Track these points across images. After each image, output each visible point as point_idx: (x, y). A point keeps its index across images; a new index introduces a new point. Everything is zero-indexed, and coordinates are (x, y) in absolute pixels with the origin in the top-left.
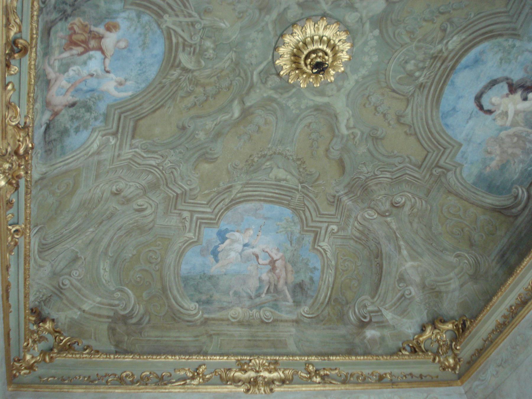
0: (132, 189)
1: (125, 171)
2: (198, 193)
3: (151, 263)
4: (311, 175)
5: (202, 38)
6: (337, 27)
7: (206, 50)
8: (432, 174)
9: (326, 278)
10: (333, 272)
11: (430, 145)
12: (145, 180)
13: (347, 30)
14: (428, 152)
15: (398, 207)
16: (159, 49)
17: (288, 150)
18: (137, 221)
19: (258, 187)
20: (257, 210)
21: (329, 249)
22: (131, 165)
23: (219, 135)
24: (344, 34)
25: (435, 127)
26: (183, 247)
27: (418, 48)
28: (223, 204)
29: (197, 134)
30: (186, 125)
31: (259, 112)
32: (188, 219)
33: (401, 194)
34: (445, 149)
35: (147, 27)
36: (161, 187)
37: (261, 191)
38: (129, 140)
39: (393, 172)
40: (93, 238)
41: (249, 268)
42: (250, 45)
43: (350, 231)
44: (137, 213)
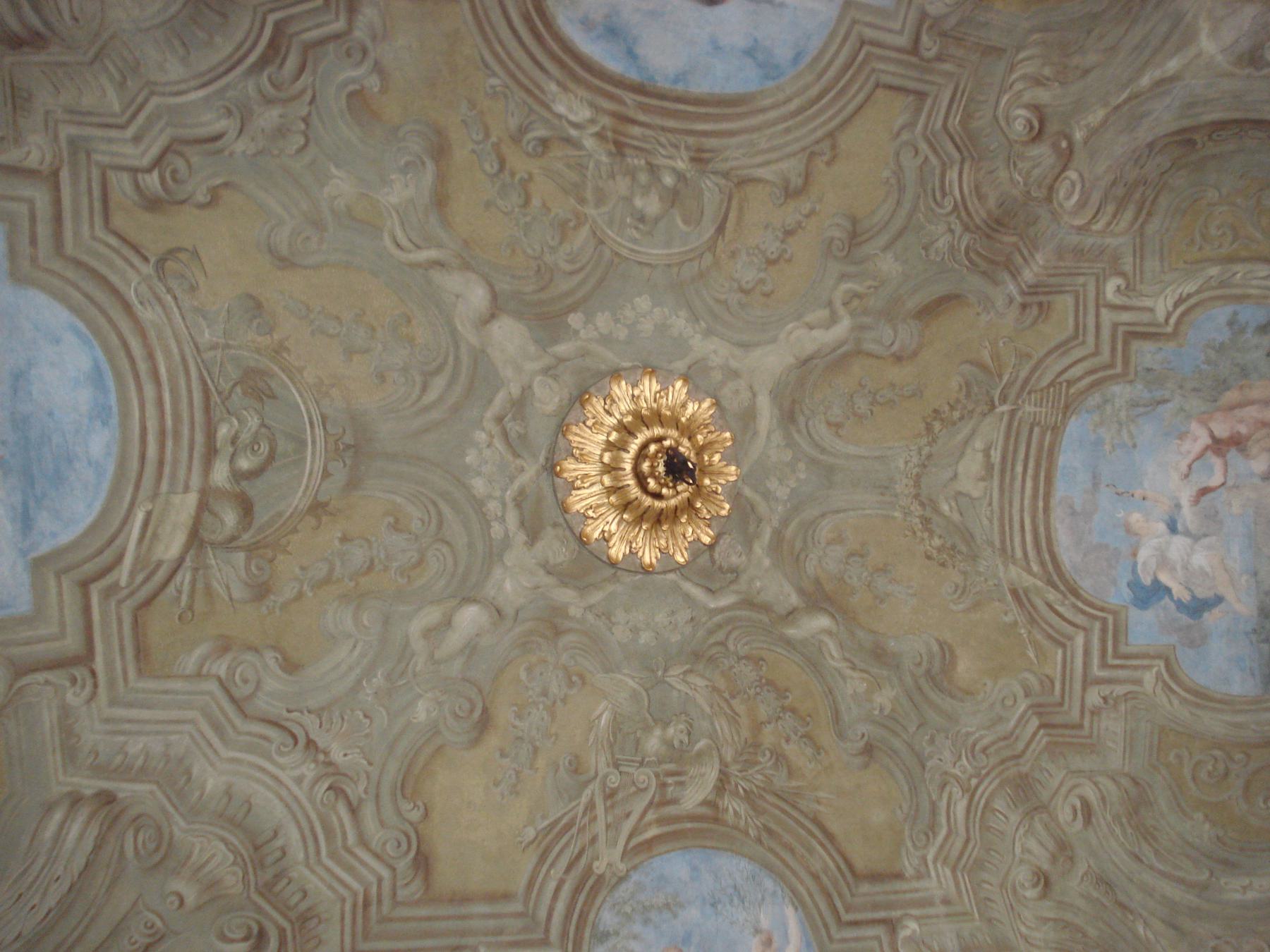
0: (1032, 844)
1: (986, 876)
2: (1035, 674)
3: (1227, 774)
4: (968, 385)
5: (641, 764)
6: (574, 429)
7: (669, 744)
8: (939, 58)
9: (1259, 287)
10: (1241, 269)
11: (856, 86)
12: (1007, 817)
13: (580, 398)
14: (877, 86)
15: (1042, 123)
16: (675, 866)
17: (906, 463)
18: (1116, 818)
19: (1011, 520)
20: (1073, 513)
21: (1174, 291)
22: (971, 861)
23: (879, 654)
24: (589, 408)
25: (807, 87)
26: (1183, 693)
27: (600, 200)
28: (1063, 604)
29: (881, 710)
30: (862, 744)
31: (811, 567)
32: (1106, 690)
33: (1003, 123)
34: (863, 43)
35: (628, 909)
36: (1025, 769)
37: (1022, 511)
38: (905, 886)
39: (944, 164)
40: (1163, 921)
41: (1236, 509)
42: (645, 637)
43: (1121, 240)
44: (1094, 820)
